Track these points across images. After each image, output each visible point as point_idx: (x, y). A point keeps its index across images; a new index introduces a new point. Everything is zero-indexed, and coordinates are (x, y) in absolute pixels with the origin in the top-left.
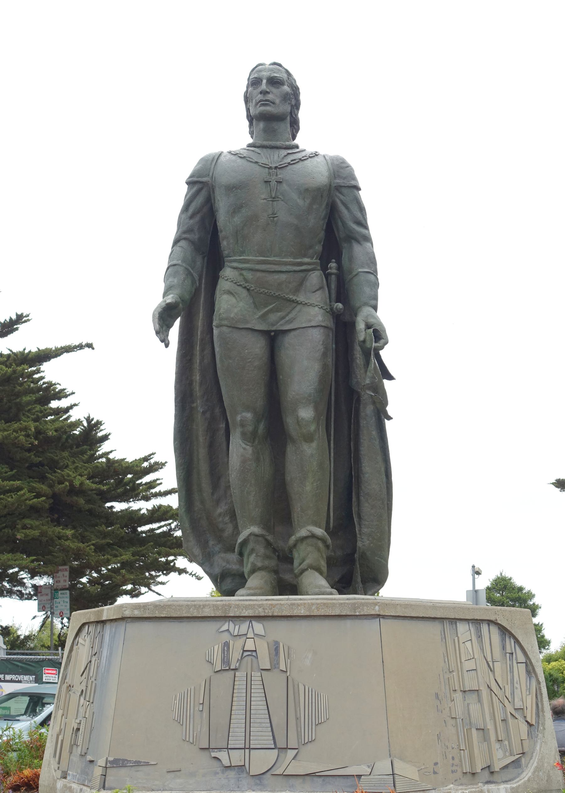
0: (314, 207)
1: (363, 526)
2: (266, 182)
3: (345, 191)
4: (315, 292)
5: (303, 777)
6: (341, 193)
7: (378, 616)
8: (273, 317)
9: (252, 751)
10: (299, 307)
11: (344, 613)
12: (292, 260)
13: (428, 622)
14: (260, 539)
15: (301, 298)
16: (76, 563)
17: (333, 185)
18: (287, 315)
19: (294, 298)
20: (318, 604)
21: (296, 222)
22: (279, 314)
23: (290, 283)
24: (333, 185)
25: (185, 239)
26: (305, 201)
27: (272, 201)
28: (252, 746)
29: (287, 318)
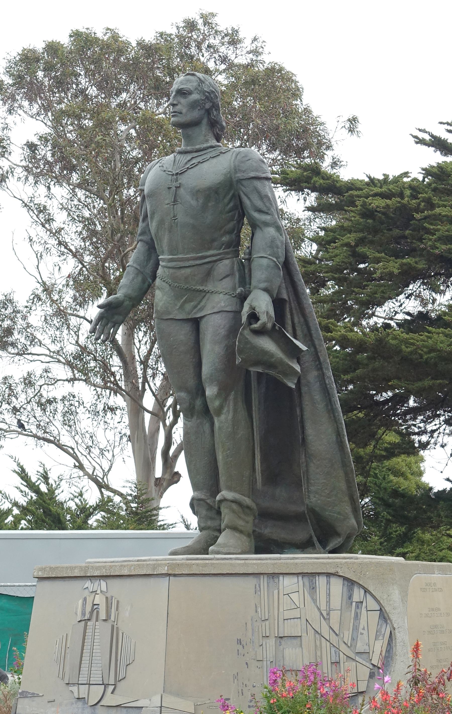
0: (210, 204)
1: (309, 485)
2: (169, 188)
3: (245, 183)
4: (221, 280)
5: (115, 708)
6: (242, 185)
7: (169, 575)
8: (188, 307)
9: (91, 686)
10: (208, 295)
11: (148, 573)
12: (194, 255)
13: (219, 578)
14: (201, 502)
15: (209, 287)
16: (367, 500)
17: (234, 180)
18: (199, 304)
19: (201, 288)
20: (135, 565)
21: (191, 221)
22: (192, 303)
23: (194, 275)
24: (234, 180)
25: (141, 240)
26: (198, 201)
27: (174, 205)
28: (91, 683)
29: (199, 307)
